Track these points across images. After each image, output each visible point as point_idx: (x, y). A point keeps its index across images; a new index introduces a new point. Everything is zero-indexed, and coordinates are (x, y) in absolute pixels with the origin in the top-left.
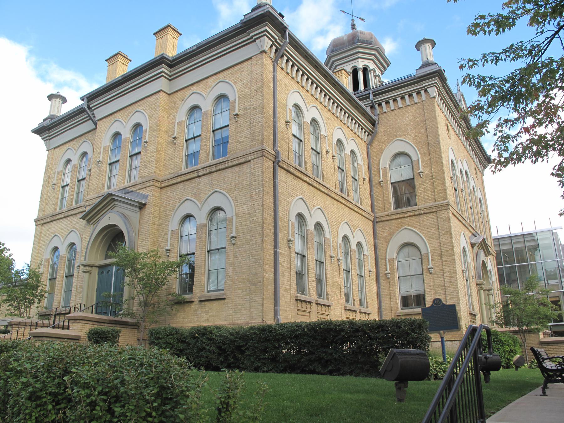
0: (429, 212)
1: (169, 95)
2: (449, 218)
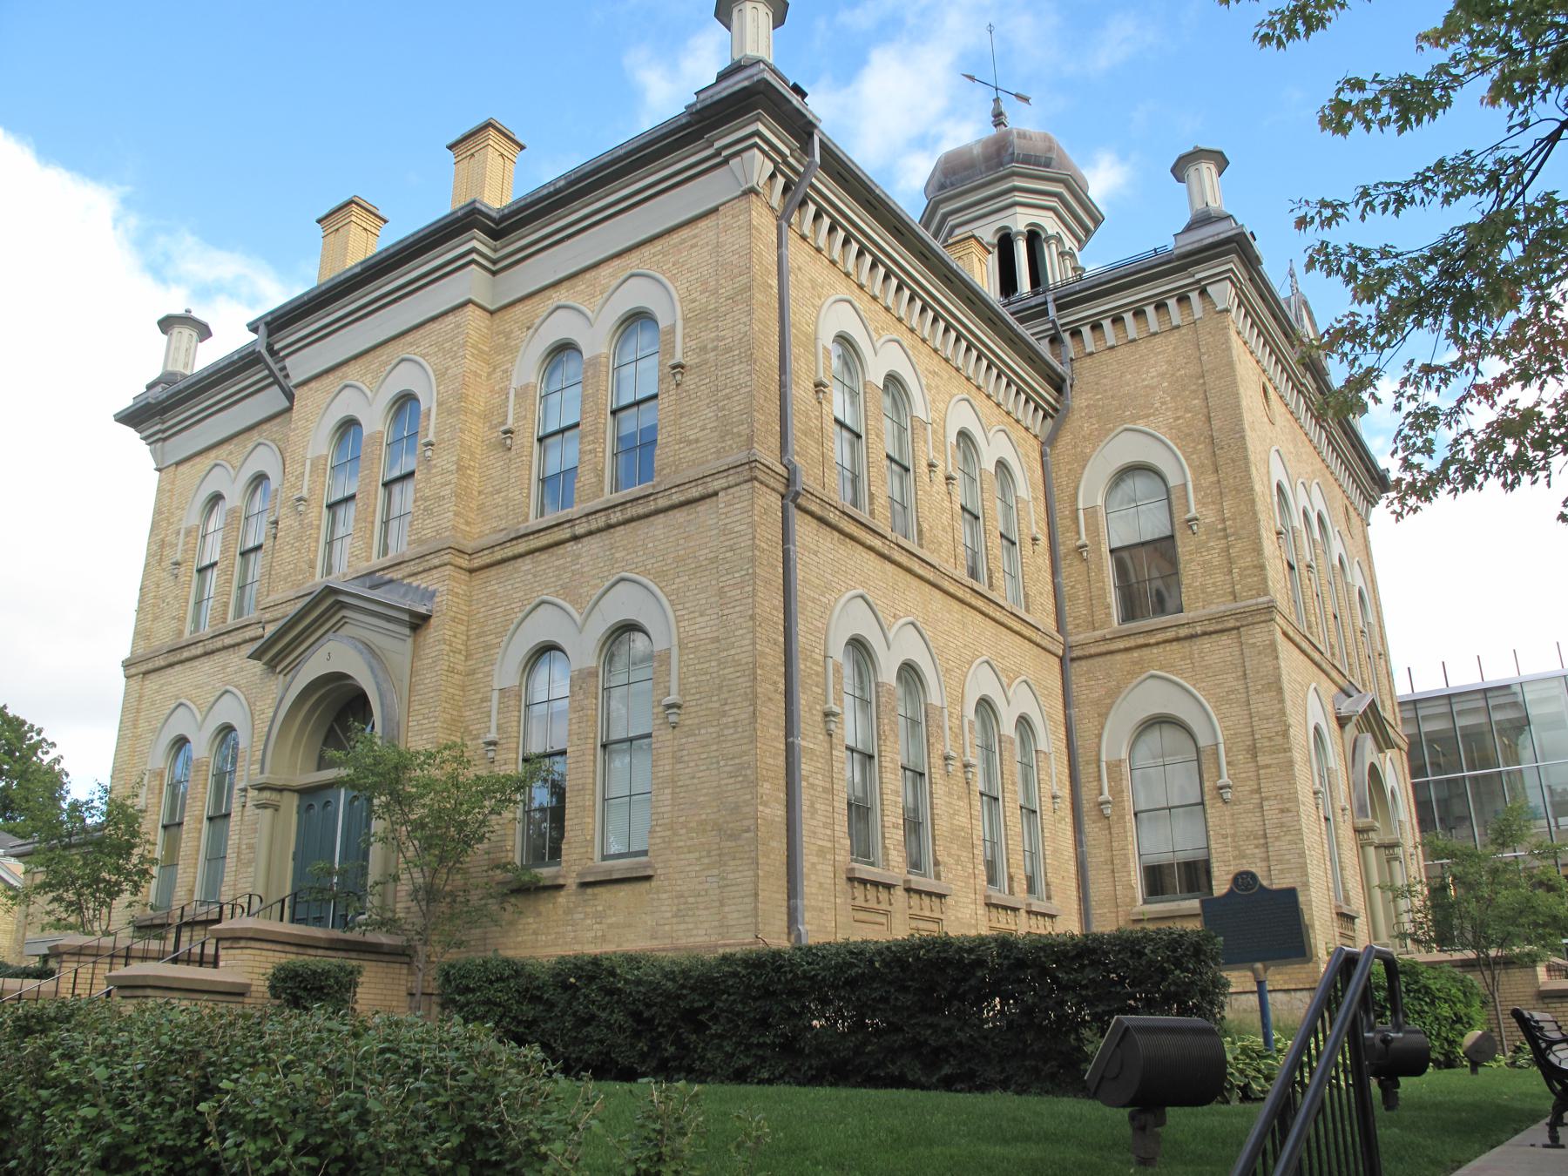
0: (1217, 628)
1: (492, 313)
2: (1273, 646)
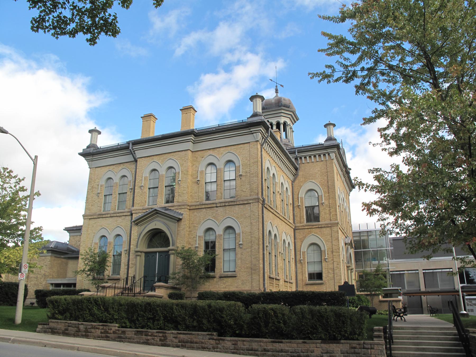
0: (327, 226)
1: (192, 152)
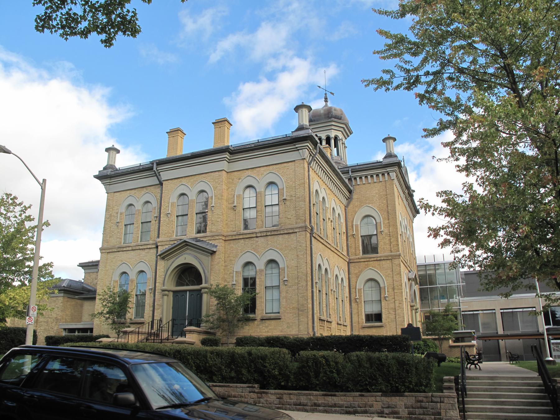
2: (400, 265)
